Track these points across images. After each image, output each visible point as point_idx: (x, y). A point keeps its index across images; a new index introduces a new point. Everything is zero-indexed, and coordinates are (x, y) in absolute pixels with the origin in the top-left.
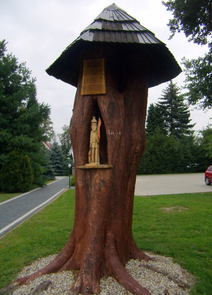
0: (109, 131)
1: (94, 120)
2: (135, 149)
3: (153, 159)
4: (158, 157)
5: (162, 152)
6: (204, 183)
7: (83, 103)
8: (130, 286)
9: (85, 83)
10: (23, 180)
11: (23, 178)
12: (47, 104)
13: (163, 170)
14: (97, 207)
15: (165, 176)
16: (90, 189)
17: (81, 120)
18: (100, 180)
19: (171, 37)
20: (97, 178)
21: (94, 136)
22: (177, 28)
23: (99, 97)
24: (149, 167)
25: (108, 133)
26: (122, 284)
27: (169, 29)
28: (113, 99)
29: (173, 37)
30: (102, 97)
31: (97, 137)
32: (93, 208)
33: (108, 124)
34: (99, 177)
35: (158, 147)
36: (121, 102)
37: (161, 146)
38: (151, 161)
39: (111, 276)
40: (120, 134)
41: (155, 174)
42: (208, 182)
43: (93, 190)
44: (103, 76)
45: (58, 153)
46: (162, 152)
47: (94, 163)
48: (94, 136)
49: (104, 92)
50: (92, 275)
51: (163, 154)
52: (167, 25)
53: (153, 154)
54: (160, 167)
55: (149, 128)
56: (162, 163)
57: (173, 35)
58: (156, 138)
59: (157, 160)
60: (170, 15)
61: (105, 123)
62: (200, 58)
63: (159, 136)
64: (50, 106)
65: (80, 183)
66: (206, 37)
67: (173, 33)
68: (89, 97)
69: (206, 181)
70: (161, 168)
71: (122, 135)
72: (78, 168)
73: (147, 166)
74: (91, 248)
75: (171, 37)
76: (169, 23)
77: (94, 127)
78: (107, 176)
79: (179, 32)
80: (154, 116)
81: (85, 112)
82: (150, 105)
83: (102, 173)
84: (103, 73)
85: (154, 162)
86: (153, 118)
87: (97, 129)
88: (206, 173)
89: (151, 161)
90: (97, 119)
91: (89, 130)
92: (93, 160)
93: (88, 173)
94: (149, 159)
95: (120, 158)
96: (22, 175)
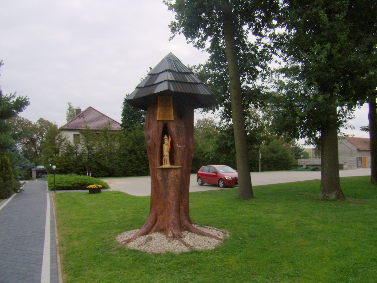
0: (178, 145)
1: (166, 137)
2: (192, 156)
3: (133, 159)
4: (139, 157)
5: (143, 152)
6: (197, 184)
7: (158, 126)
8: (200, 233)
9: (159, 112)
10: (3, 184)
11: (4, 182)
12: (26, 96)
13: (144, 171)
14: (174, 191)
15: (132, 179)
16: (167, 181)
17: (158, 137)
18: (175, 175)
19: (172, 38)
20: (172, 174)
21: (166, 148)
22: (178, 30)
23: (169, 122)
24: (128, 168)
25: (177, 147)
26: (194, 233)
27: (170, 30)
28: (178, 124)
29: (173, 38)
30: (171, 122)
31: (168, 148)
32: (171, 193)
33: (177, 141)
34: (173, 173)
35: (138, 146)
36: (183, 126)
37: (141, 144)
38: (130, 161)
39: (186, 230)
40: (184, 146)
41: (135, 176)
42: (201, 183)
43: (169, 181)
44: (172, 109)
45: (15, 151)
46: (143, 152)
47: (167, 165)
48: (166, 148)
49: (173, 120)
50: (178, 229)
51: (144, 153)
52: (169, 26)
53: (132, 153)
54: (141, 168)
55: (125, 124)
56: (143, 164)
57: (173, 36)
58: (135, 135)
59: (137, 161)
60: (172, 16)
61: (175, 140)
62: (201, 65)
63: (139, 133)
64: (29, 99)
65: (160, 178)
66: (205, 42)
67: (173, 35)
68: (162, 121)
69: (199, 181)
70: (142, 169)
71: (185, 147)
72: (158, 168)
73: (126, 167)
74: (173, 215)
75: (172, 38)
76: (170, 25)
77: (166, 141)
78: (179, 173)
79: (179, 34)
80: (131, 110)
81: (160, 132)
82: (127, 95)
83: (175, 171)
84: (172, 106)
85: (134, 162)
86: (130, 111)
87: (168, 143)
88: (199, 173)
89: (130, 161)
90: (168, 137)
91: (162, 142)
92: (166, 163)
93: (165, 171)
94: (128, 159)
95: (185, 162)
96: (2, 179)
